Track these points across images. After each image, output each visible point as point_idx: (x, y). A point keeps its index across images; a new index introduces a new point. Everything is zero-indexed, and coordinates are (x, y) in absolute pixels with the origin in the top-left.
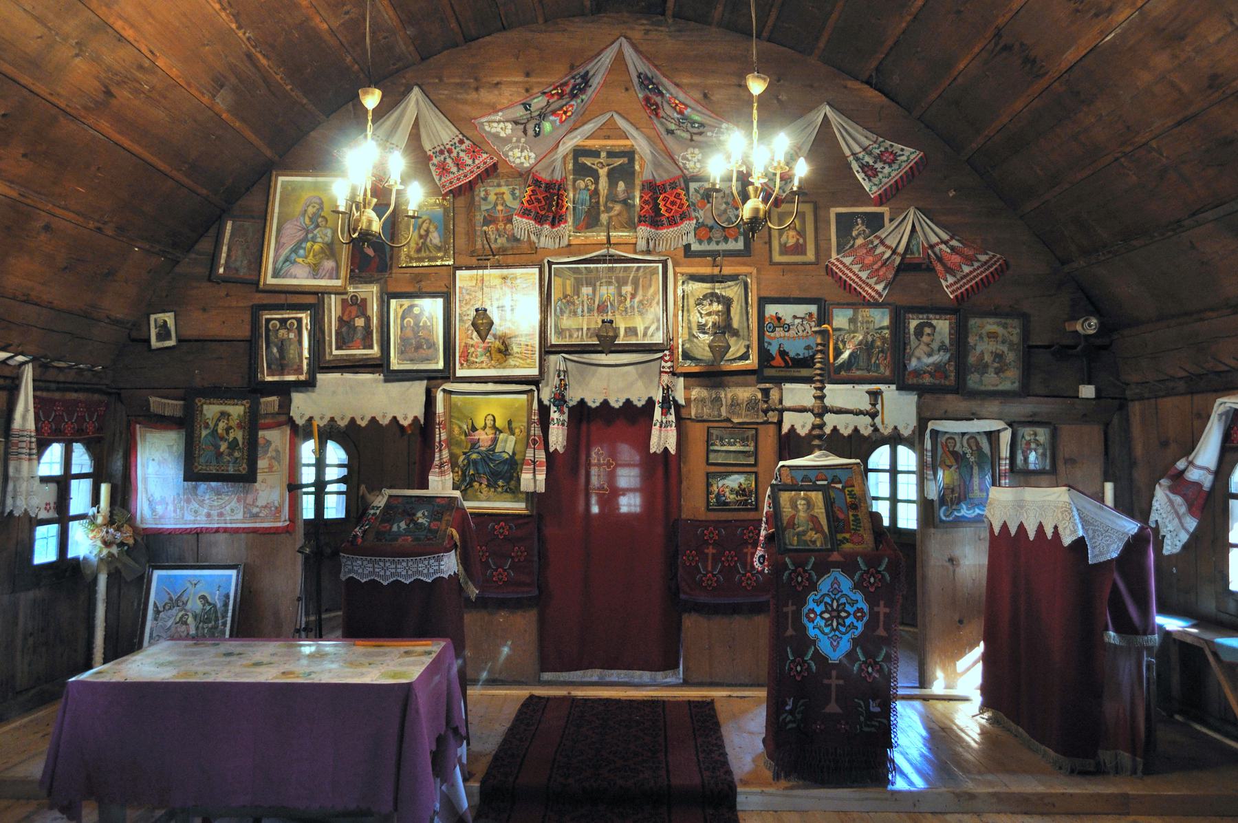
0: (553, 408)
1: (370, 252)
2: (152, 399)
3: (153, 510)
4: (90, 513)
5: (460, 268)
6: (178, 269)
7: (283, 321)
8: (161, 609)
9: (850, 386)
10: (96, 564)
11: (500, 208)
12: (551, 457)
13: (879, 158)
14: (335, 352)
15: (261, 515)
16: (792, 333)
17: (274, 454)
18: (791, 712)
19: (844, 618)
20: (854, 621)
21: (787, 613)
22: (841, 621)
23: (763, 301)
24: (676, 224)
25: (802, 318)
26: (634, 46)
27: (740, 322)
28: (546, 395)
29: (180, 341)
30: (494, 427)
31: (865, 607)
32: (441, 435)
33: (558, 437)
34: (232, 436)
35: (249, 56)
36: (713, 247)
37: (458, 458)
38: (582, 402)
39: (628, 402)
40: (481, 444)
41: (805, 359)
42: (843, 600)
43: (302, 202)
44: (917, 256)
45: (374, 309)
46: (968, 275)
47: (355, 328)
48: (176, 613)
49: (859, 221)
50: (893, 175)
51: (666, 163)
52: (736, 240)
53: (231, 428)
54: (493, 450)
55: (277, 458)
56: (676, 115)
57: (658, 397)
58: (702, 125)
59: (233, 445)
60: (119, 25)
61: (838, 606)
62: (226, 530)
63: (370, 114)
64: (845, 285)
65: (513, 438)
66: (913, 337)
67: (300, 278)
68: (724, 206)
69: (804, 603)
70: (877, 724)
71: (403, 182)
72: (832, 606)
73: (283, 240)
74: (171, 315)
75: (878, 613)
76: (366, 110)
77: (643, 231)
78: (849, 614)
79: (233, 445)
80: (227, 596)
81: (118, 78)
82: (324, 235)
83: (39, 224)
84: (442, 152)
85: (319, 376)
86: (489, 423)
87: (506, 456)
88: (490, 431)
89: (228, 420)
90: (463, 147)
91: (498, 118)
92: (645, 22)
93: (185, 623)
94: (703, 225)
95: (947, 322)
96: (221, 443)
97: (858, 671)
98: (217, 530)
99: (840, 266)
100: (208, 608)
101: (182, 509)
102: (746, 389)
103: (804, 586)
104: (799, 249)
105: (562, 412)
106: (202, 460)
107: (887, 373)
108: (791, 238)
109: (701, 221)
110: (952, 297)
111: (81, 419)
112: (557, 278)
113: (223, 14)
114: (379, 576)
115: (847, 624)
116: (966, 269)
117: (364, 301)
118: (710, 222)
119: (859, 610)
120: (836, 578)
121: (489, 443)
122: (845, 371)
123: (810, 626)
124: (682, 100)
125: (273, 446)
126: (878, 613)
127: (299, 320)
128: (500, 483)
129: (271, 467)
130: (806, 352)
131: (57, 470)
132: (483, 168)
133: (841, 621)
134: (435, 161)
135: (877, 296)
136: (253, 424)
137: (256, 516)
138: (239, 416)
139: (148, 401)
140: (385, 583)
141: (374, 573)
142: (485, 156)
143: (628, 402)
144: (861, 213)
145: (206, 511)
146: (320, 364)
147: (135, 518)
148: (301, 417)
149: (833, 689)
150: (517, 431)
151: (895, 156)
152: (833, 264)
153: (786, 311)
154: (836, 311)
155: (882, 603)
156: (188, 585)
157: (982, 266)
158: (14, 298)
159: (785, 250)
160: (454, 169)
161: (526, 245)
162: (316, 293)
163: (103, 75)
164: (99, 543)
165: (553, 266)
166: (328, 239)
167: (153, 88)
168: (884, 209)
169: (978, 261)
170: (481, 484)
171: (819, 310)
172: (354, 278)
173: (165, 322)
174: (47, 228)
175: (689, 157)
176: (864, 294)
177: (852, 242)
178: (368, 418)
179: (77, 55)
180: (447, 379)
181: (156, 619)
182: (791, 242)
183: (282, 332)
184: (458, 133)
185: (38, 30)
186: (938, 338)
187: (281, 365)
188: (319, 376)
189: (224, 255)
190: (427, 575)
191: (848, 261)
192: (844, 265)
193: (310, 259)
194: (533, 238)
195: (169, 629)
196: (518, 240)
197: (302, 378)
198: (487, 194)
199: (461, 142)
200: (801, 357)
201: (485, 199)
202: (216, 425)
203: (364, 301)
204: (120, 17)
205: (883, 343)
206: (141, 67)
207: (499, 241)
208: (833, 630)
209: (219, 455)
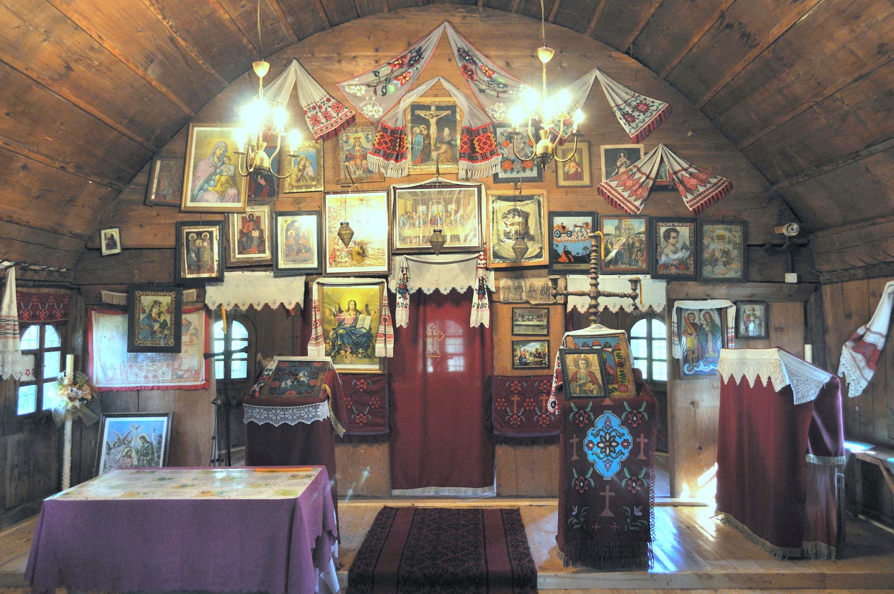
0: (398, 295)
1: (262, 182)
2: (104, 292)
3: (105, 374)
4: (59, 377)
5: (328, 193)
6: (121, 197)
7: (199, 234)
8: (112, 446)
9: (616, 276)
10: (63, 414)
11: (357, 148)
12: (397, 331)
13: (636, 108)
14: (238, 256)
15: (185, 376)
16: (574, 237)
17: (194, 332)
18: (577, 516)
20: (622, 449)
22: (612, 449)
23: (552, 215)
24: (487, 159)
25: (581, 227)
27: (536, 230)
28: (393, 285)
29: (123, 249)
30: (355, 309)
31: (630, 439)
32: (316, 316)
33: (402, 317)
35: (172, 40)
36: (515, 175)
38: (420, 290)
39: (454, 290)
40: (346, 322)
41: (583, 257)
42: (613, 434)
43: (212, 146)
44: (664, 180)
45: (265, 224)
46: (702, 193)
47: (252, 238)
48: (123, 449)
49: (622, 155)
52: (532, 170)
53: (162, 312)
54: (355, 327)
55: (196, 334)
56: (486, 79)
57: (476, 286)
58: (505, 86)
59: (164, 325)
60: (75, 17)
62: (159, 388)
64: (612, 202)
65: (369, 318)
66: (662, 240)
67: (211, 202)
68: (522, 145)
69: (585, 436)
70: (640, 524)
71: (286, 130)
72: (605, 438)
73: (199, 174)
74: (117, 230)
75: (639, 443)
77: (463, 164)
78: (618, 444)
79: (164, 325)
80: (161, 437)
83: (20, 164)
84: (314, 108)
85: (227, 274)
86: (352, 307)
87: (364, 331)
88: (352, 313)
89: (159, 307)
90: (330, 104)
92: (462, 10)
93: (130, 457)
95: (688, 228)
96: (155, 324)
98: (153, 388)
99: (608, 188)
100: (147, 445)
101: (126, 372)
102: (541, 279)
104: (578, 176)
106: (141, 337)
107: (644, 266)
108: (572, 168)
109: (505, 156)
110: (691, 209)
111: (51, 308)
112: (400, 200)
114: (272, 420)
115: (617, 451)
116: (701, 189)
117: (258, 218)
119: (625, 441)
120: (608, 418)
121: (352, 321)
123: (589, 453)
126: (639, 443)
127: (211, 233)
129: (191, 341)
130: (584, 251)
131: (35, 346)
132: (345, 119)
135: (635, 210)
136: (178, 309)
137: (181, 377)
138: (167, 304)
139: (100, 294)
140: (277, 425)
143: (454, 290)
145: (144, 374)
146: (227, 265)
147: (92, 379)
148: (213, 304)
149: (607, 499)
150: (372, 312)
152: (603, 186)
155: (642, 435)
156: (132, 428)
157: (713, 186)
159: (567, 177)
160: (324, 120)
161: (377, 176)
162: (223, 213)
163: (64, 54)
164: (66, 399)
165: (397, 191)
166: (231, 173)
167: (101, 63)
169: (710, 183)
170: (346, 352)
171: (593, 220)
172: (251, 201)
173: (112, 236)
174: (24, 167)
175: (496, 109)
176: (626, 208)
178: (262, 304)
179: (45, 40)
180: (320, 274)
181: (108, 454)
182: (572, 171)
183: (199, 242)
184: (326, 93)
185: (16, 22)
186: (681, 240)
187: (198, 266)
188: (227, 274)
190: (307, 419)
191: (614, 184)
192: (611, 187)
193: (219, 188)
194: (382, 170)
195: (118, 461)
196: (371, 172)
197: (214, 275)
198: (348, 138)
199: (328, 100)
200: (581, 255)
201: (347, 142)
202: (151, 310)
203: (258, 218)
204: (76, 11)
205: (641, 244)
206: (92, 48)
207: (357, 173)
208: (606, 455)
209: (153, 333)
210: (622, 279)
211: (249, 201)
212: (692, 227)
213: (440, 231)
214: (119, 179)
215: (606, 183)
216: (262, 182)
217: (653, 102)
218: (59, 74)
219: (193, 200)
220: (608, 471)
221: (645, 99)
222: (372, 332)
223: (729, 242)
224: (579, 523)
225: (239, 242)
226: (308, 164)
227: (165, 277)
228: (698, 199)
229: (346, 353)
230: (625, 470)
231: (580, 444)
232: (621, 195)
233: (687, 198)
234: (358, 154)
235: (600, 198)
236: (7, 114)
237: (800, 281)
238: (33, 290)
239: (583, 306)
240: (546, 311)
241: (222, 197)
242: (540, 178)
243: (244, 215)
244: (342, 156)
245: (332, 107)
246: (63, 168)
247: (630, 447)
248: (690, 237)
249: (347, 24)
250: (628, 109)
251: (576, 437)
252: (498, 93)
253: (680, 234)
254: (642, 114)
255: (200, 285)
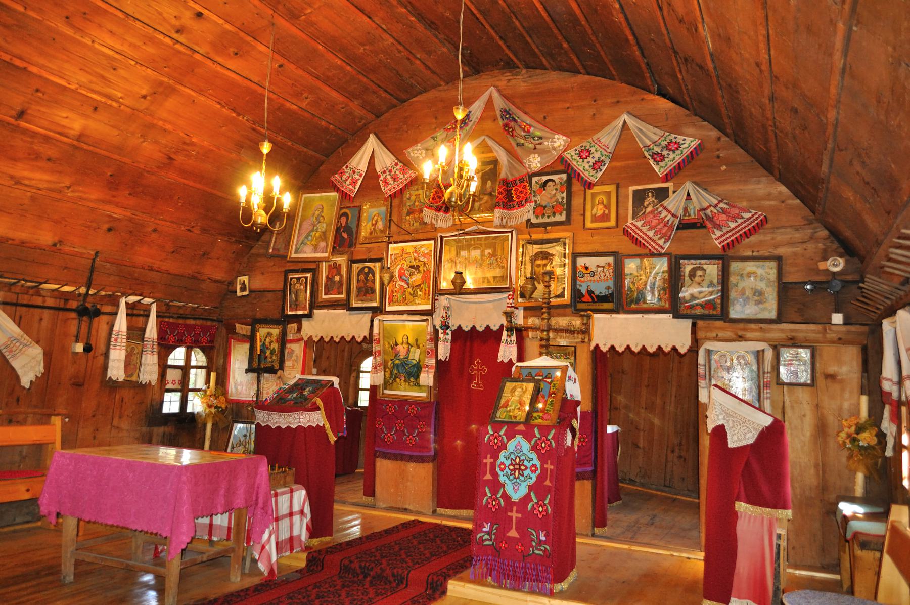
1: (345, 235)
2: (237, 325)
3: (237, 389)
5: (391, 243)
6: (253, 251)
7: (298, 279)
9: (640, 316)
11: (417, 203)
12: (439, 363)
13: (667, 147)
14: (324, 297)
16: (596, 277)
18: (489, 533)
19: (523, 470)
20: (530, 473)
21: (486, 464)
22: (521, 472)
23: (575, 256)
24: (522, 206)
26: (499, 91)
28: (438, 322)
29: (250, 291)
30: (408, 343)
31: (538, 464)
33: (444, 351)
34: (272, 346)
35: (254, 129)
36: (545, 220)
37: (388, 363)
38: (460, 327)
39: (488, 327)
40: (400, 354)
41: (606, 296)
42: (523, 458)
43: (313, 209)
44: (693, 217)
45: (344, 270)
46: (733, 229)
49: (650, 194)
50: (677, 159)
51: (518, 166)
52: (561, 214)
53: (272, 342)
54: (407, 358)
56: (523, 133)
58: (541, 138)
59: (273, 352)
60: (160, 123)
61: (520, 461)
63: (265, 156)
64: (636, 242)
65: (418, 351)
66: (687, 278)
67: (308, 253)
68: (554, 191)
69: (498, 457)
70: (543, 548)
71: (280, 193)
72: (515, 461)
73: (302, 232)
74: (247, 277)
76: (263, 154)
77: (498, 212)
78: (527, 468)
79: (273, 352)
81: (174, 150)
82: (322, 227)
83: (150, 229)
84: (384, 172)
85: (316, 311)
86: (405, 340)
87: (415, 362)
88: (406, 346)
90: (398, 168)
91: (418, 148)
92: (508, 74)
94: (540, 205)
95: (716, 266)
97: (532, 509)
99: (634, 228)
101: (250, 389)
102: (565, 318)
103: (499, 446)
104: (605, 217)
105: (446, 334)
107: (667, 306)
108: (599, 211)
109: (538, 203)
110: (720, 246)
113: (224, 110)
115: (525, 475)
116: (732, 225)
117: (340, 265)
118: (544, 204)
119: (534, 466)
120: (519, 442)
121: (405, 353)
122: (635, 304)
123: (501, 473)
124: (528, 122)
125: (295, 354)
127: (306, 278)
128: (412, 379)
129: (293, 365)
130: (607, 291)
132: (409, 179)
133: (521, 472)
134: (382, 178)
135: (659, 249)
136: (283, 341)
140: (273, 427)
141: (268, 421)
142: (410, 172)
143: (488, 327)
144: (651, 189)
146: (315, 304)
149: (514, 519)
150: (421, 346)
151: (678, 145)
152: (629, 227)
153: (592, 262)
154: (627, 261)
157: (745, 222)
158: (143, 268)
159: (595, 219)
160: (391, 182)
161: (429, 227)
162: (315, 262)
163: (163, 150)
164: (205, 405)
166: (324, 230)
167: (198, 153)
168: (670, 185)
169: (743, 218)
171: (615, 260)
172: (334, 251)
174: (155, 230)
175: (532, 160)
176: (650, 247)
177: (644, 210)
178: (340, 337)
179: (144, 142)
180: (381, 313)
182: (600, 213)
184: (394, 159)
185: (116, 132)
186: (707, 278)
187: (296, 305)
188: (316, 311)
189: (273, 242)
190: (293, 424)
191: (639, 224)
192: (637, 227)
193: (314, 242)
194: (434, 221)
196: (425, 223)
197: (306, 312)
198: (411, 195)
199: (396, 164)
200: (603, 294)
201: (409, 199)
203: (340, 265)
204: (161, 119)
206: (184, 143)
207: (415, 225)
208: (515, 477)
210: (646, 318)
211: (333, 251)
212: (721, 265)
213: (461, 273)
214: (247, 238)
215: (632, 223)
216: (345, 235)
217: (684, 140)
218: (164, 164)
219: (296, 253)
220: (515, 492)
221: (676, 138)
222: (421, 363)
223: (762, 280)
224: (491, 540)
225: (325, 286)
226: (379, 220)
227: (276, 315)
228: (727, 236)
229: (401, 382)
230: (532, 494)
231: (493, 465)
232: (646, 235)
233: (715, 234)
234: (417, 208)
235: (627, 238)
236: (130, 194)
237: (846, 323)
238: (181, 321)
239: (605, 345)
240: (574, 348)
241: (316, 250)
242: (568, 221)
243: (330, 263)
244: (405, 211)
245: (400, 170)
246: (189, 230)
247: (538, 472)
248: (718, 275)
249: (414, 99)
250: (657, 149)
251: (491, 458)
252: (535, 145)
253: (707, 272)
254: (671, 153)
255: (298, 319)
